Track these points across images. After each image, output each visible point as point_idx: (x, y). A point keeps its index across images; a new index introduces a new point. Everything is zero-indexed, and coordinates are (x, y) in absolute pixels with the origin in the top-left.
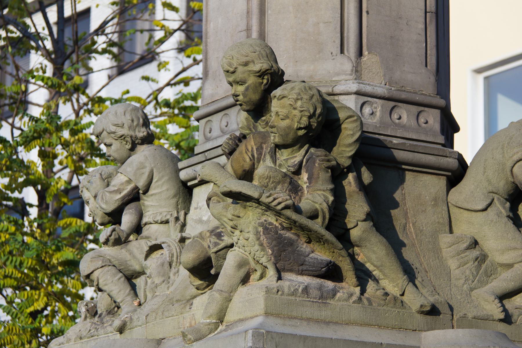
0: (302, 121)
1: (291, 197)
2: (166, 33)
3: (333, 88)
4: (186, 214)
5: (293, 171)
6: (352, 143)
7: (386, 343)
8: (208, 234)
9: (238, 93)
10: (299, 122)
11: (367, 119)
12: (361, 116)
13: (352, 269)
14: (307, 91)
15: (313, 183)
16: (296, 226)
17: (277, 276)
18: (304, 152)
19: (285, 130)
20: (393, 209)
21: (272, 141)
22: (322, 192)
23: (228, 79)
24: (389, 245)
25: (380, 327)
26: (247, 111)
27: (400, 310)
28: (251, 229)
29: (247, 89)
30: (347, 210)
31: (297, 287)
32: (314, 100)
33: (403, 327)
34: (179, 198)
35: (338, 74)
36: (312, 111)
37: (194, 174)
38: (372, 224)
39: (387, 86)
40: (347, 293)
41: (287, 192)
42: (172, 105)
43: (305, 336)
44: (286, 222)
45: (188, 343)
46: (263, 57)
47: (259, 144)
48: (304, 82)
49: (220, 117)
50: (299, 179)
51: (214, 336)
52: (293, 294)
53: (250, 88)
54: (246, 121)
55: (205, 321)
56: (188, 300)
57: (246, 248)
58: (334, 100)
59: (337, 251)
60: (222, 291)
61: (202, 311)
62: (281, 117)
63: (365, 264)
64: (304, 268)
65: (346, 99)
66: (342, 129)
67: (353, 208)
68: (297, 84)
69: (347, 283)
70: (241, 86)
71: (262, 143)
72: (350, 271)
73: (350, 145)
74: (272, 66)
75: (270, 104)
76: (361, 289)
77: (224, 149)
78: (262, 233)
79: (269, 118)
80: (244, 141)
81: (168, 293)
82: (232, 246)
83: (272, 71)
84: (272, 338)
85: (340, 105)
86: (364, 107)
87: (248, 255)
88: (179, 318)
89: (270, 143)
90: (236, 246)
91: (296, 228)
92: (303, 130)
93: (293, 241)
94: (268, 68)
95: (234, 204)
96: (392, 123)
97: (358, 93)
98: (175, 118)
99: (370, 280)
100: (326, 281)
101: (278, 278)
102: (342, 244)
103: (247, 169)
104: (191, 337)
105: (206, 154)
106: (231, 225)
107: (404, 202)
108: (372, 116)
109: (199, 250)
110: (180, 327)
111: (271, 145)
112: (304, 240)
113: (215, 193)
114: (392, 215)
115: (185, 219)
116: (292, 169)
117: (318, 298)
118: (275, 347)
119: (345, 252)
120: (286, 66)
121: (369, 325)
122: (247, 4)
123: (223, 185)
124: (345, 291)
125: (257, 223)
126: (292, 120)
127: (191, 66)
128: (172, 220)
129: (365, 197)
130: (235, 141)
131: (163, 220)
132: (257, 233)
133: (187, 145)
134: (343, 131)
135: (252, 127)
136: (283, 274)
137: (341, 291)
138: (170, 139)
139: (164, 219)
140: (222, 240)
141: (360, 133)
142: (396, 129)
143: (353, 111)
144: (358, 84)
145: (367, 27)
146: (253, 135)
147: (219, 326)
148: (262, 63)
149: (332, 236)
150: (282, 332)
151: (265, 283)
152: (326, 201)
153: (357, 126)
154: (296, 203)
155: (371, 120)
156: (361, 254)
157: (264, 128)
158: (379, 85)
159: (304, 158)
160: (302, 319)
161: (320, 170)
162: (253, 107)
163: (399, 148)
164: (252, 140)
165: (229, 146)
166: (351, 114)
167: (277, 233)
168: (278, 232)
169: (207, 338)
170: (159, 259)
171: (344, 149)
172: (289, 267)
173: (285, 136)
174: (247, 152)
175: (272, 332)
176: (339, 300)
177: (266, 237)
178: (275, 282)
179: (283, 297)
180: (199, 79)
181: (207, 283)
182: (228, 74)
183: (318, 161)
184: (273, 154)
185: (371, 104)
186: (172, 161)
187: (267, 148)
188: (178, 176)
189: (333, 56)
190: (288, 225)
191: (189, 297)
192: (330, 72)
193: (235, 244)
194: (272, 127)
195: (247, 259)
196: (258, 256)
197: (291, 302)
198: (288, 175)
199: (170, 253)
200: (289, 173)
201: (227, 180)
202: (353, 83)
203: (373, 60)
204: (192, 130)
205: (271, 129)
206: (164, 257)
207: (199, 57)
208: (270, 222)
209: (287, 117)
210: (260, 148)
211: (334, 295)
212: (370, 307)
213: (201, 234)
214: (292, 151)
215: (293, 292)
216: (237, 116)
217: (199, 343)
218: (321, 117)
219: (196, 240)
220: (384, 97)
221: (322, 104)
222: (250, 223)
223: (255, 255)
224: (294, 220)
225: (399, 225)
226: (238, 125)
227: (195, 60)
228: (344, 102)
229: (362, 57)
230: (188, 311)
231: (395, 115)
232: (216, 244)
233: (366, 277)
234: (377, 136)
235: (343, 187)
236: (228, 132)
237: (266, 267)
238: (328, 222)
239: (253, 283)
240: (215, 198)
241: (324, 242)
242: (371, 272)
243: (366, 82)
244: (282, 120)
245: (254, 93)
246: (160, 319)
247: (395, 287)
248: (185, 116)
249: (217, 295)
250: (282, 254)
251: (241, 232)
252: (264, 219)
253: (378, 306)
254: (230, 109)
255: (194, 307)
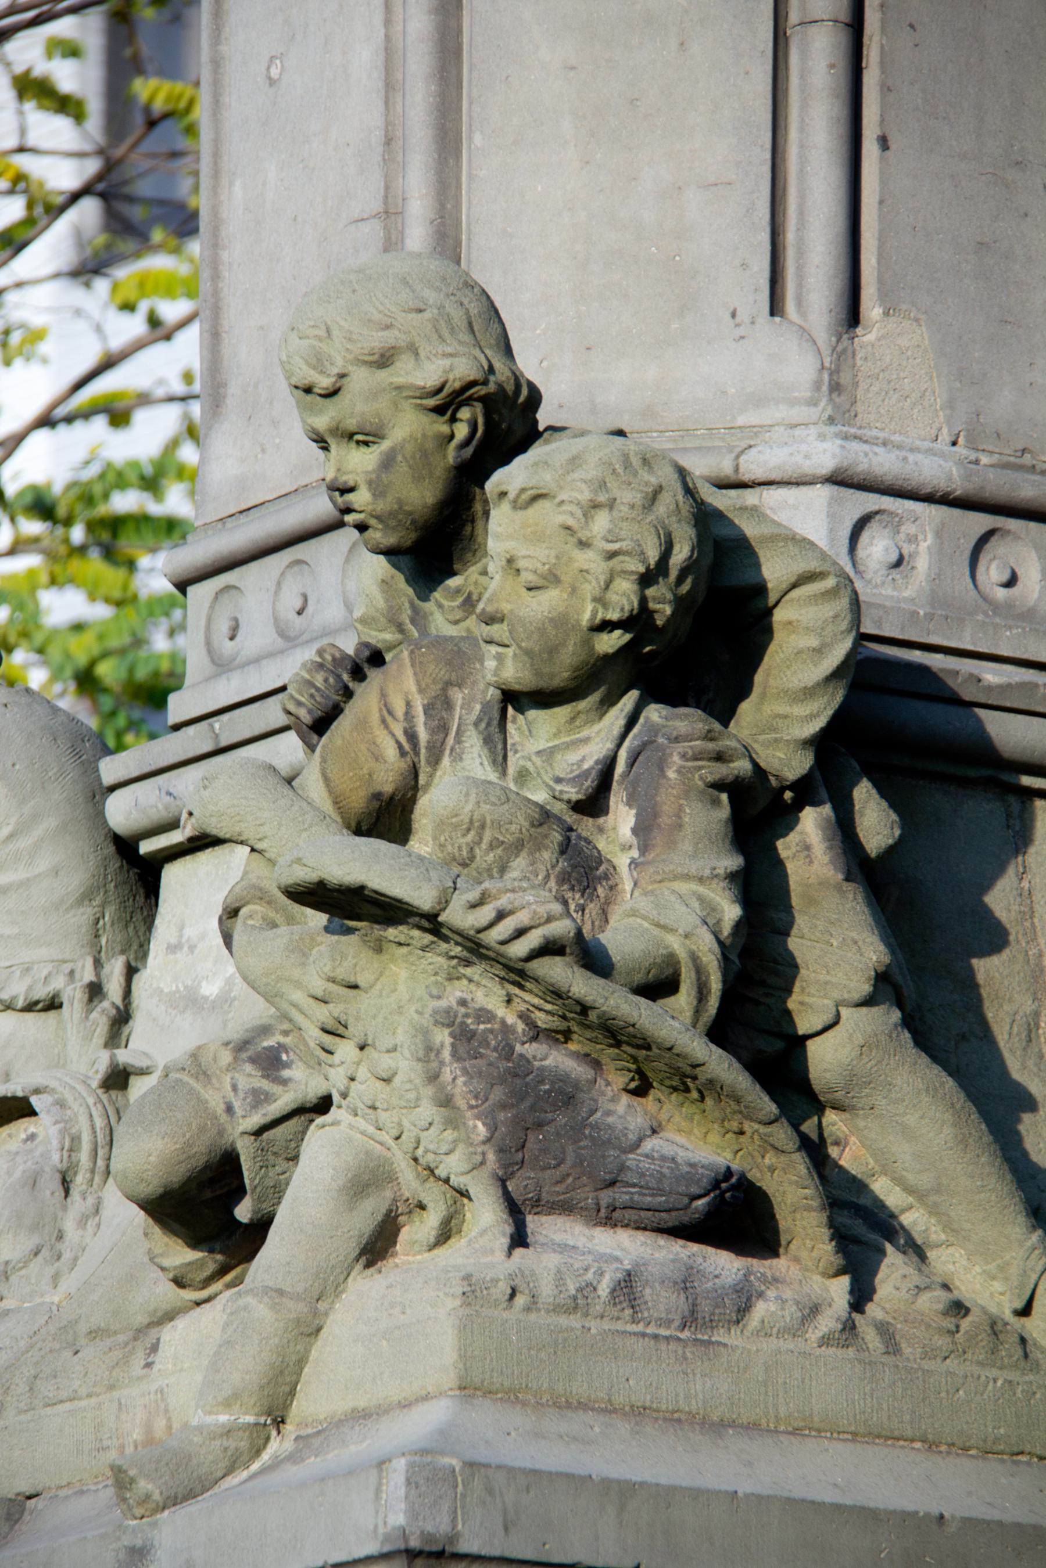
0: (612, 597)
1: (565, 903)
2: (30, 205)
3: (738, 457)
4: (131, 972)
5: (575, 797)
6: (818, 685)
7: (958, 1514)
8: (226, 1057)
9: (349, 479)
10: (600, 600)
11: (876, 586)
12: (852, 574)
13: (815, 1203)
14: (635, 474)
15: (658, 850)
16: (588, 1027)
17: (509, 1229)
18: (622, 722)
19: (542, 631)
20: (983, 953)
21: (490, 677)
22: (694, 886)
23: (310, 421)
24: (969, 1104)
25: (931, 1445)
26: (389, 553)
27: (1014, 1376)
28: (402, 1036)
29: (387, 462)
30: (793, 958)
31: (590, 1276)
32: (662, 508)
33: (1028, 1448)
34: (103, 905)
35: (759, 401)
36: (653, 555)
37: (166, 808)
38: (896, 1015)
39: (961, 450)
40: (797, 1303)
41: (552, 883)
42: (61, 511)
43: (626, 1482)
44: (548, 1007)
45: (139, 1512)
46: (452, 331)
47: (435, 689)
48: (620, 433)
49: (276, 573)
50: (601, 830)
51: (249, 1485)
52: (576, 1308)
53: (400, 458)
54: (383, 592)
55: (210, 1419)
56: (139, 1331)
57: (383, 1116)
58: (743, 509)
59: (756, 1126)
60: (281, 1292)
61: (199, 1378)
62: (527, 577)
63: (868, 1181)
64: (620, 1195)
65: (791, 501)
66: (776, 626)
67: (817, 952)
68: (591, 441)
69: (797, 1260)
70: (363, 449)
71: (448, 684)
72: (809, 1209)
73: (808, 693)
74: (491, 370)
75: (480, 524)
76: (852, 1284)
77: (291, 707)
78: (446, 1054)
79: (476, 583)
80: (374, 675)
81: (56, 1299)
82: (324, 1105)
83: (492, 387)
84: (489, 1490)
85: (766, 530)
86: (865, 537)
87: (391, 1142)
88: (99, 1406)
89: (481, 686)
90: (339, 1107)
91: (589, 1034)
92: (618, 633)
93: (576, 1086)
94: (474, 374)
95: (333, 933)
96: (980, 601)
97: (840, 479)
98: (75, 565)
99: (889, 1248)
100: (710, 1250)
101: (512, 1237)
102: (774, 1099)
103: (388, 788)
104: (150, 1486)
105: (217, 726)
106: (322, 1018)
107: (1027, 924)
108: (895, 574)
109: (190, 1124)
110: (105, 1443)
111: (485, 692)
112: (619, 1080)
113: (254, 887)
114: (981, 977)
115: (127, 992)
116: (574, 793)
117: (677, 1323)
118: (501, 1528)
119: (790, 1130)
120: (545, 364)
121: (887, 1438)
122: (386, 103)
123: (289, 857)
124: (788, 1294)
125: (429, 1011)
126: (574, 590)
127: (138, 346)
128: (74, 996)
129: (869, 904)
130: (338, 677)
131: (36, 998)
132: (430, 1051)
133: (123, 674)
134: (779, 635)
135: (405, 617)
136: (536, 1224)
137: (771, 1294)
138: (55, 652)
139: (41, 993)
140: (284, 1082)
141: (847, 644)
142: (996, 626)
143: (823, 553)
144: (839, 442)
145: (881, 202)
146: (412, 652)
147: (268, 1439)
148: (451, 355)
149: (736, 1065)
150: (528, 1464)
151: (460, 1261)
152: (711, 921)
153: (836, 616)
154: (586, 931)
155: (895, 589)
156: (853, 1139)
157: (456, 622)
158: (927, 444)
159: (619, 746)
160: (610, 1410)
161: (687, 794)
162: (413, 536)
163: (1008, 704)
164: (409, 671)
165: (312, 696)
166: (813, 565)
167: (508, 1052)
168: (512, 1049)
169: (216, 1489)
170: (19, 1159)
171: (783, 709)
172: (558, 1193)
173: (545, 656)
174: (389, 719)
175: (487, 1466)
176: (764, 1331)
177: (465, 1071)
178: (500, 1255)
179: (533, 1316)
180: (171, 399)
181: (219, 1257)
182: (309, 398)
183: (676, 758)
184: (494, 729)
185: (895, 522)
186: (76, 752)
187: (467, 705)
188: (100, 814)
189: (737, 325)
190: (555, 1023)
191: (141, 1319)
192: (724, 393)
193: (336, 1098)
194: (490, 620)
195: (386, 1160)
196: (431, 1147)
197: (565, 1340)
198: (556, 816)
199: (63, 1132)
200: (558, 808)
201: (305, 835)
202: (822, 437)
203: (904, 342)
204: (144, 612)
205: (486, 630)
206: (40, 1149)
207: (172, 310)
208: (482, 1009)
209: (552, 579)
210: (439, 705)
211: (743, 1310)
212: (890, 1359)
213: (195, 1056)
214: (573, 719)
215: (575, 1298)
216: (344, 571)
217: (183, 1512)
218: (689, 581)
219: (177, 1080)
220: (947, 494)
221: (695, 526)
222: (400, 1010)
223: (418, 1142)
224: (578, 1002)
225: (1008, 1020)
226: (349, 607)
227: (154, 321)
228: (782, 517)
229: (859, 330)
230: (140, 1379)
231: (994, 566)
232: (259, 1098)
233: (874, 1237)
234: (916, 656)
235: (779, 864)
236: (306, 636)
237: (464, 1194)
238: (719, 1009)
239: (410, 1258)
240: (257, 907)
241: (700, 1092)
242: (893, 1216)
243: (875, 433)
244: (530, 589)
245: (418, 479)
246: (21, 1412)
247: (994, 1278)
248: (109, 554)
249: (260, 1310)
250: (531, 1137)
251: (362, 1048)
252: (458, 994)
253: (925, 1355)
254: (313, 543)
255: (164, 1359)
